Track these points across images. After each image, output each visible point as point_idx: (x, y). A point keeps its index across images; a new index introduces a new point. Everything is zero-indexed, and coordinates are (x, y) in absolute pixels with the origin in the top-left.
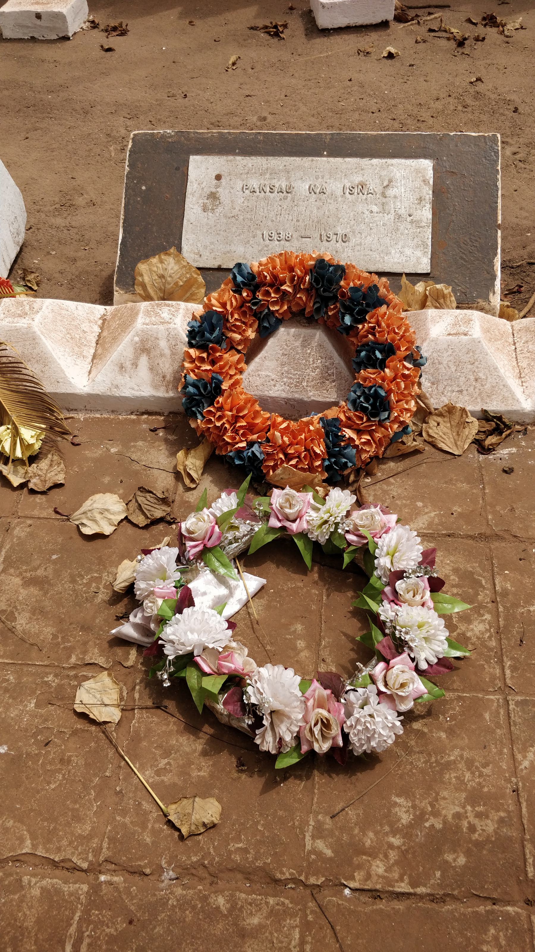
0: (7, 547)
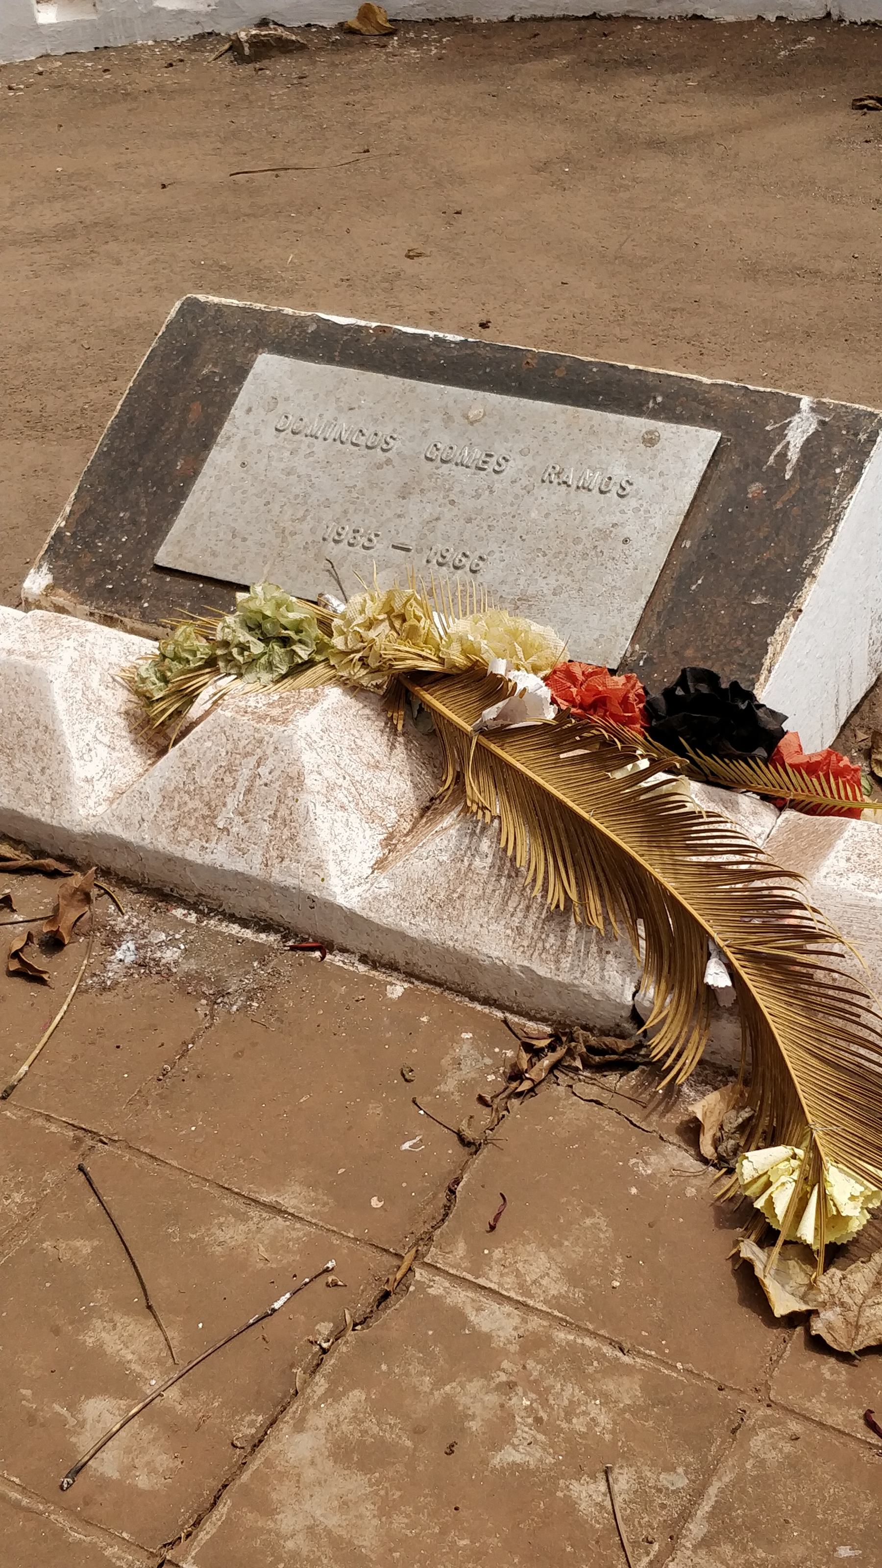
0: (726, 1479)
